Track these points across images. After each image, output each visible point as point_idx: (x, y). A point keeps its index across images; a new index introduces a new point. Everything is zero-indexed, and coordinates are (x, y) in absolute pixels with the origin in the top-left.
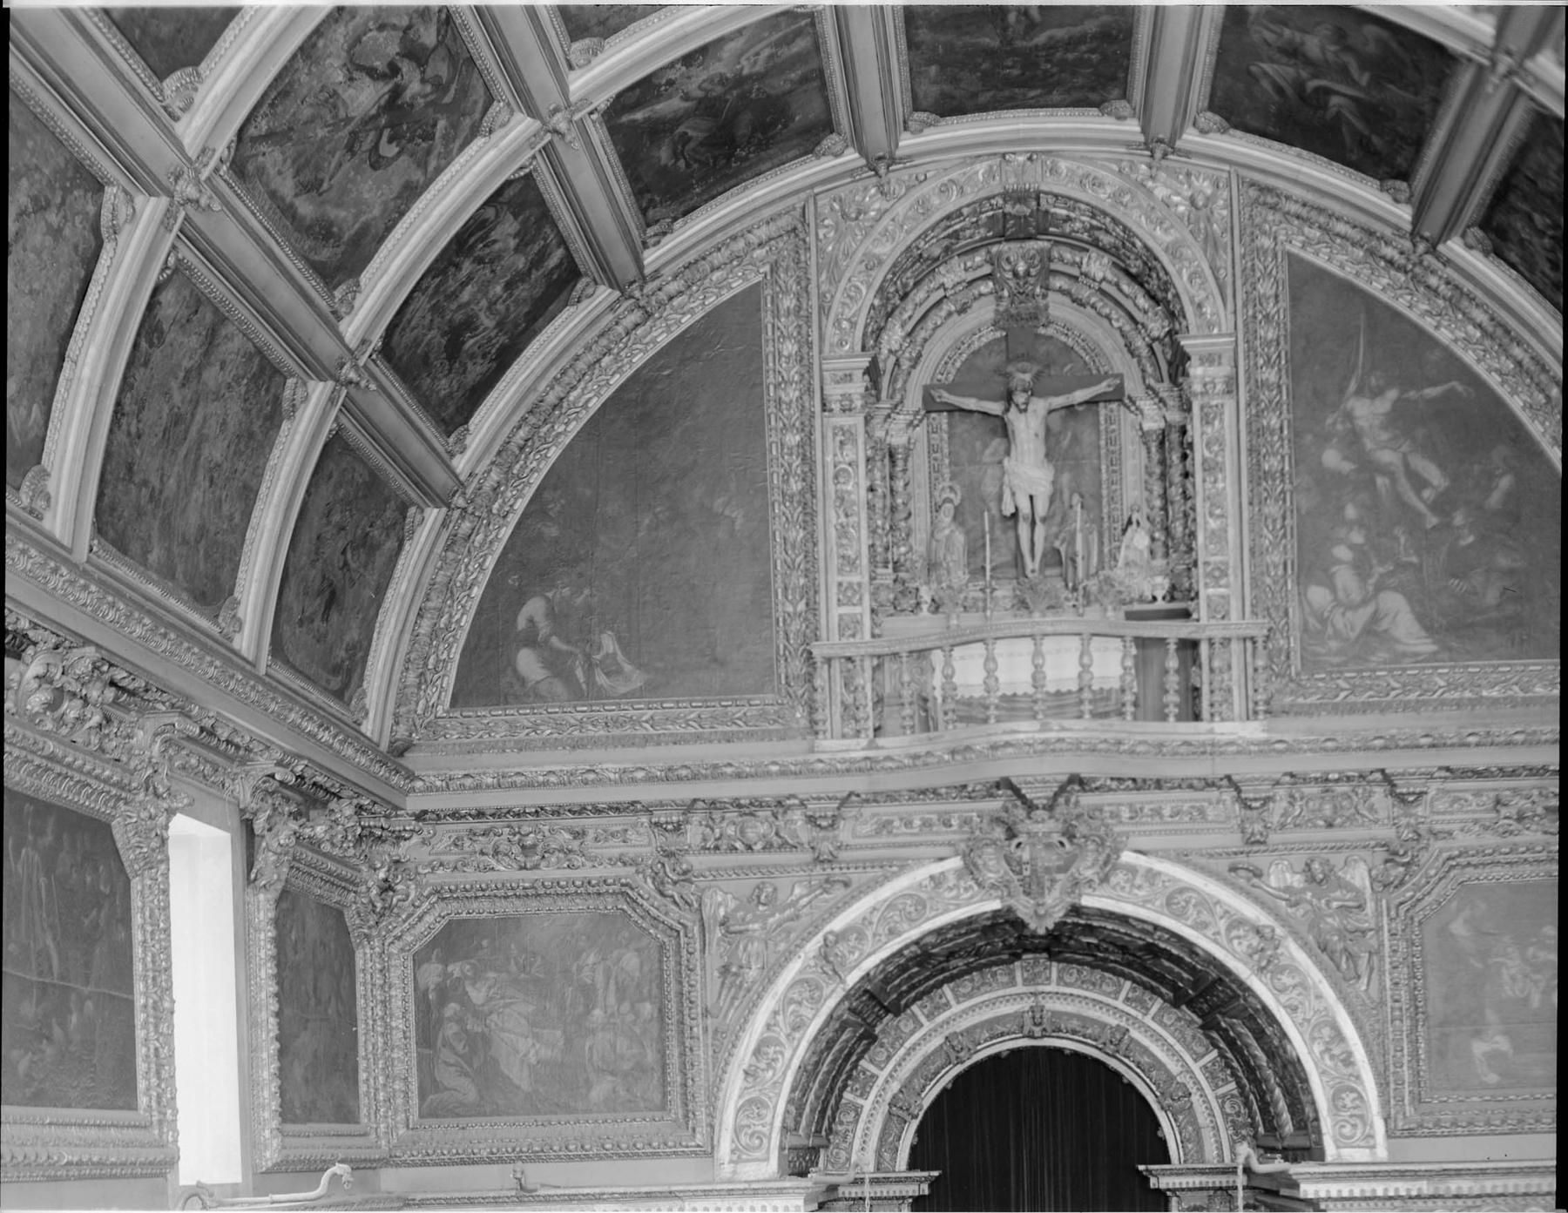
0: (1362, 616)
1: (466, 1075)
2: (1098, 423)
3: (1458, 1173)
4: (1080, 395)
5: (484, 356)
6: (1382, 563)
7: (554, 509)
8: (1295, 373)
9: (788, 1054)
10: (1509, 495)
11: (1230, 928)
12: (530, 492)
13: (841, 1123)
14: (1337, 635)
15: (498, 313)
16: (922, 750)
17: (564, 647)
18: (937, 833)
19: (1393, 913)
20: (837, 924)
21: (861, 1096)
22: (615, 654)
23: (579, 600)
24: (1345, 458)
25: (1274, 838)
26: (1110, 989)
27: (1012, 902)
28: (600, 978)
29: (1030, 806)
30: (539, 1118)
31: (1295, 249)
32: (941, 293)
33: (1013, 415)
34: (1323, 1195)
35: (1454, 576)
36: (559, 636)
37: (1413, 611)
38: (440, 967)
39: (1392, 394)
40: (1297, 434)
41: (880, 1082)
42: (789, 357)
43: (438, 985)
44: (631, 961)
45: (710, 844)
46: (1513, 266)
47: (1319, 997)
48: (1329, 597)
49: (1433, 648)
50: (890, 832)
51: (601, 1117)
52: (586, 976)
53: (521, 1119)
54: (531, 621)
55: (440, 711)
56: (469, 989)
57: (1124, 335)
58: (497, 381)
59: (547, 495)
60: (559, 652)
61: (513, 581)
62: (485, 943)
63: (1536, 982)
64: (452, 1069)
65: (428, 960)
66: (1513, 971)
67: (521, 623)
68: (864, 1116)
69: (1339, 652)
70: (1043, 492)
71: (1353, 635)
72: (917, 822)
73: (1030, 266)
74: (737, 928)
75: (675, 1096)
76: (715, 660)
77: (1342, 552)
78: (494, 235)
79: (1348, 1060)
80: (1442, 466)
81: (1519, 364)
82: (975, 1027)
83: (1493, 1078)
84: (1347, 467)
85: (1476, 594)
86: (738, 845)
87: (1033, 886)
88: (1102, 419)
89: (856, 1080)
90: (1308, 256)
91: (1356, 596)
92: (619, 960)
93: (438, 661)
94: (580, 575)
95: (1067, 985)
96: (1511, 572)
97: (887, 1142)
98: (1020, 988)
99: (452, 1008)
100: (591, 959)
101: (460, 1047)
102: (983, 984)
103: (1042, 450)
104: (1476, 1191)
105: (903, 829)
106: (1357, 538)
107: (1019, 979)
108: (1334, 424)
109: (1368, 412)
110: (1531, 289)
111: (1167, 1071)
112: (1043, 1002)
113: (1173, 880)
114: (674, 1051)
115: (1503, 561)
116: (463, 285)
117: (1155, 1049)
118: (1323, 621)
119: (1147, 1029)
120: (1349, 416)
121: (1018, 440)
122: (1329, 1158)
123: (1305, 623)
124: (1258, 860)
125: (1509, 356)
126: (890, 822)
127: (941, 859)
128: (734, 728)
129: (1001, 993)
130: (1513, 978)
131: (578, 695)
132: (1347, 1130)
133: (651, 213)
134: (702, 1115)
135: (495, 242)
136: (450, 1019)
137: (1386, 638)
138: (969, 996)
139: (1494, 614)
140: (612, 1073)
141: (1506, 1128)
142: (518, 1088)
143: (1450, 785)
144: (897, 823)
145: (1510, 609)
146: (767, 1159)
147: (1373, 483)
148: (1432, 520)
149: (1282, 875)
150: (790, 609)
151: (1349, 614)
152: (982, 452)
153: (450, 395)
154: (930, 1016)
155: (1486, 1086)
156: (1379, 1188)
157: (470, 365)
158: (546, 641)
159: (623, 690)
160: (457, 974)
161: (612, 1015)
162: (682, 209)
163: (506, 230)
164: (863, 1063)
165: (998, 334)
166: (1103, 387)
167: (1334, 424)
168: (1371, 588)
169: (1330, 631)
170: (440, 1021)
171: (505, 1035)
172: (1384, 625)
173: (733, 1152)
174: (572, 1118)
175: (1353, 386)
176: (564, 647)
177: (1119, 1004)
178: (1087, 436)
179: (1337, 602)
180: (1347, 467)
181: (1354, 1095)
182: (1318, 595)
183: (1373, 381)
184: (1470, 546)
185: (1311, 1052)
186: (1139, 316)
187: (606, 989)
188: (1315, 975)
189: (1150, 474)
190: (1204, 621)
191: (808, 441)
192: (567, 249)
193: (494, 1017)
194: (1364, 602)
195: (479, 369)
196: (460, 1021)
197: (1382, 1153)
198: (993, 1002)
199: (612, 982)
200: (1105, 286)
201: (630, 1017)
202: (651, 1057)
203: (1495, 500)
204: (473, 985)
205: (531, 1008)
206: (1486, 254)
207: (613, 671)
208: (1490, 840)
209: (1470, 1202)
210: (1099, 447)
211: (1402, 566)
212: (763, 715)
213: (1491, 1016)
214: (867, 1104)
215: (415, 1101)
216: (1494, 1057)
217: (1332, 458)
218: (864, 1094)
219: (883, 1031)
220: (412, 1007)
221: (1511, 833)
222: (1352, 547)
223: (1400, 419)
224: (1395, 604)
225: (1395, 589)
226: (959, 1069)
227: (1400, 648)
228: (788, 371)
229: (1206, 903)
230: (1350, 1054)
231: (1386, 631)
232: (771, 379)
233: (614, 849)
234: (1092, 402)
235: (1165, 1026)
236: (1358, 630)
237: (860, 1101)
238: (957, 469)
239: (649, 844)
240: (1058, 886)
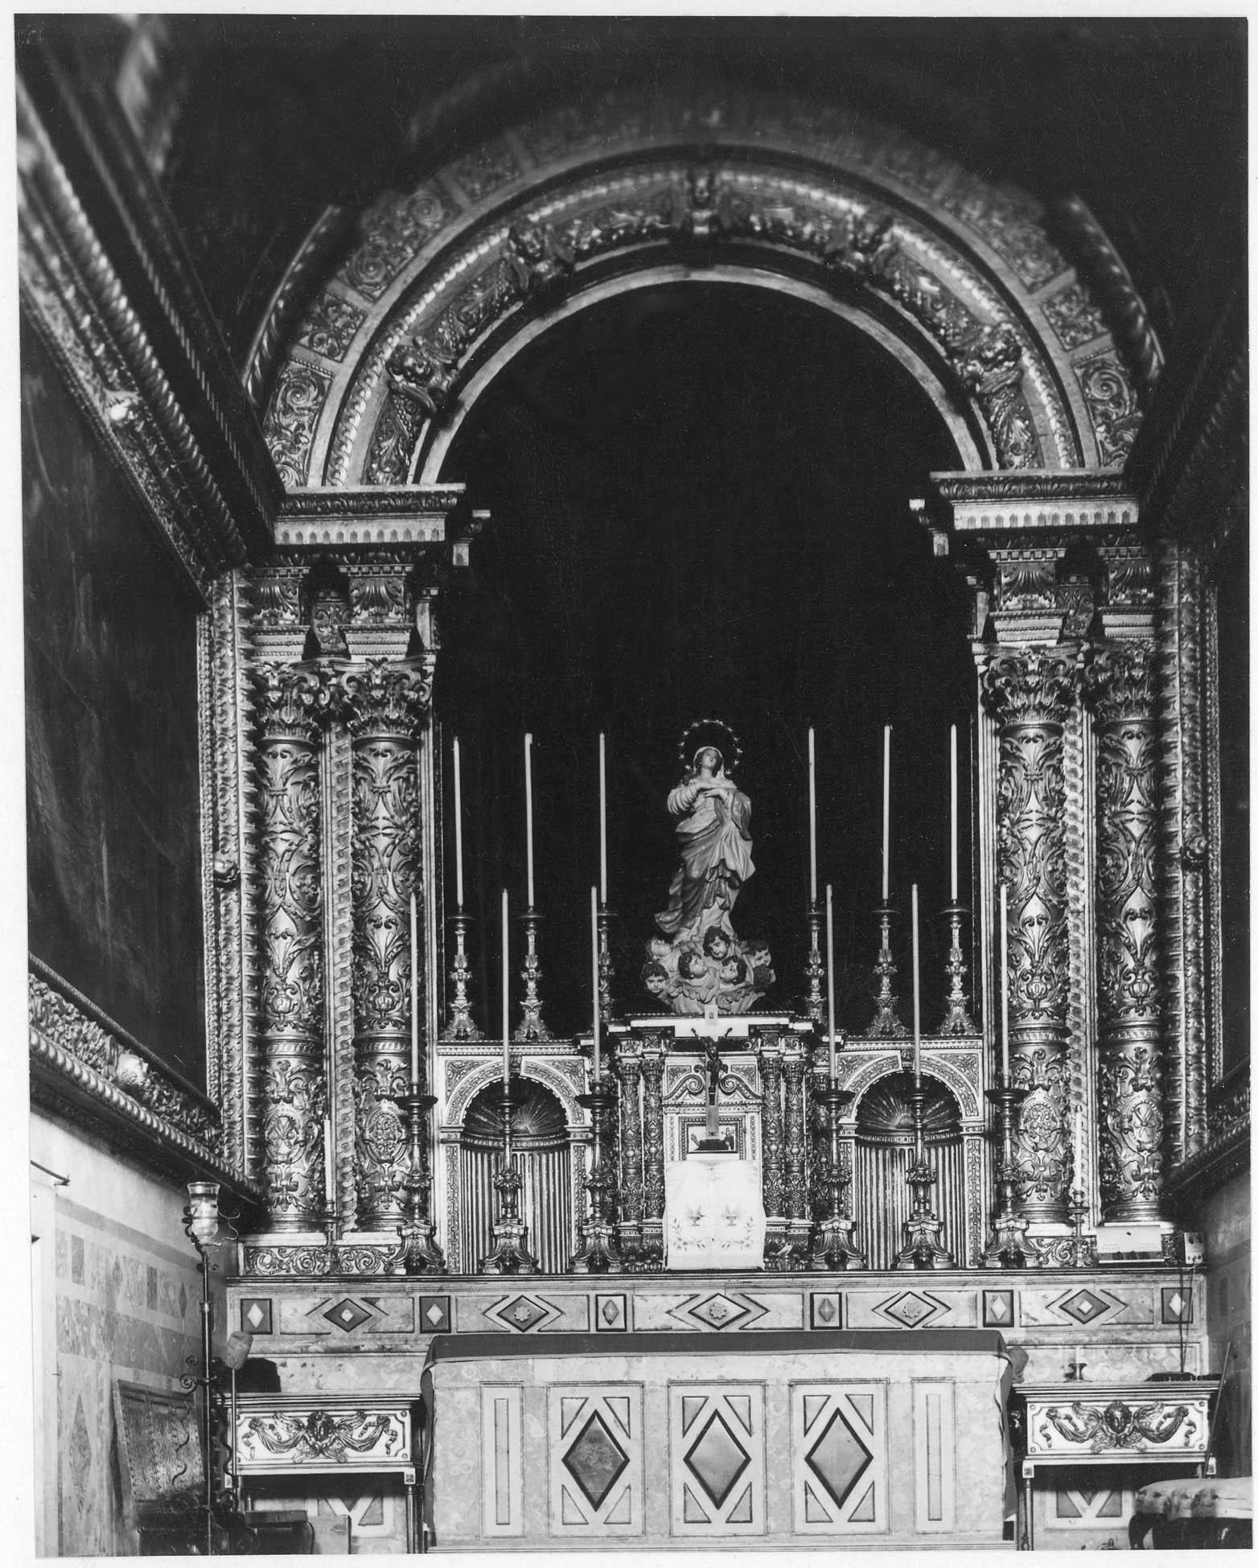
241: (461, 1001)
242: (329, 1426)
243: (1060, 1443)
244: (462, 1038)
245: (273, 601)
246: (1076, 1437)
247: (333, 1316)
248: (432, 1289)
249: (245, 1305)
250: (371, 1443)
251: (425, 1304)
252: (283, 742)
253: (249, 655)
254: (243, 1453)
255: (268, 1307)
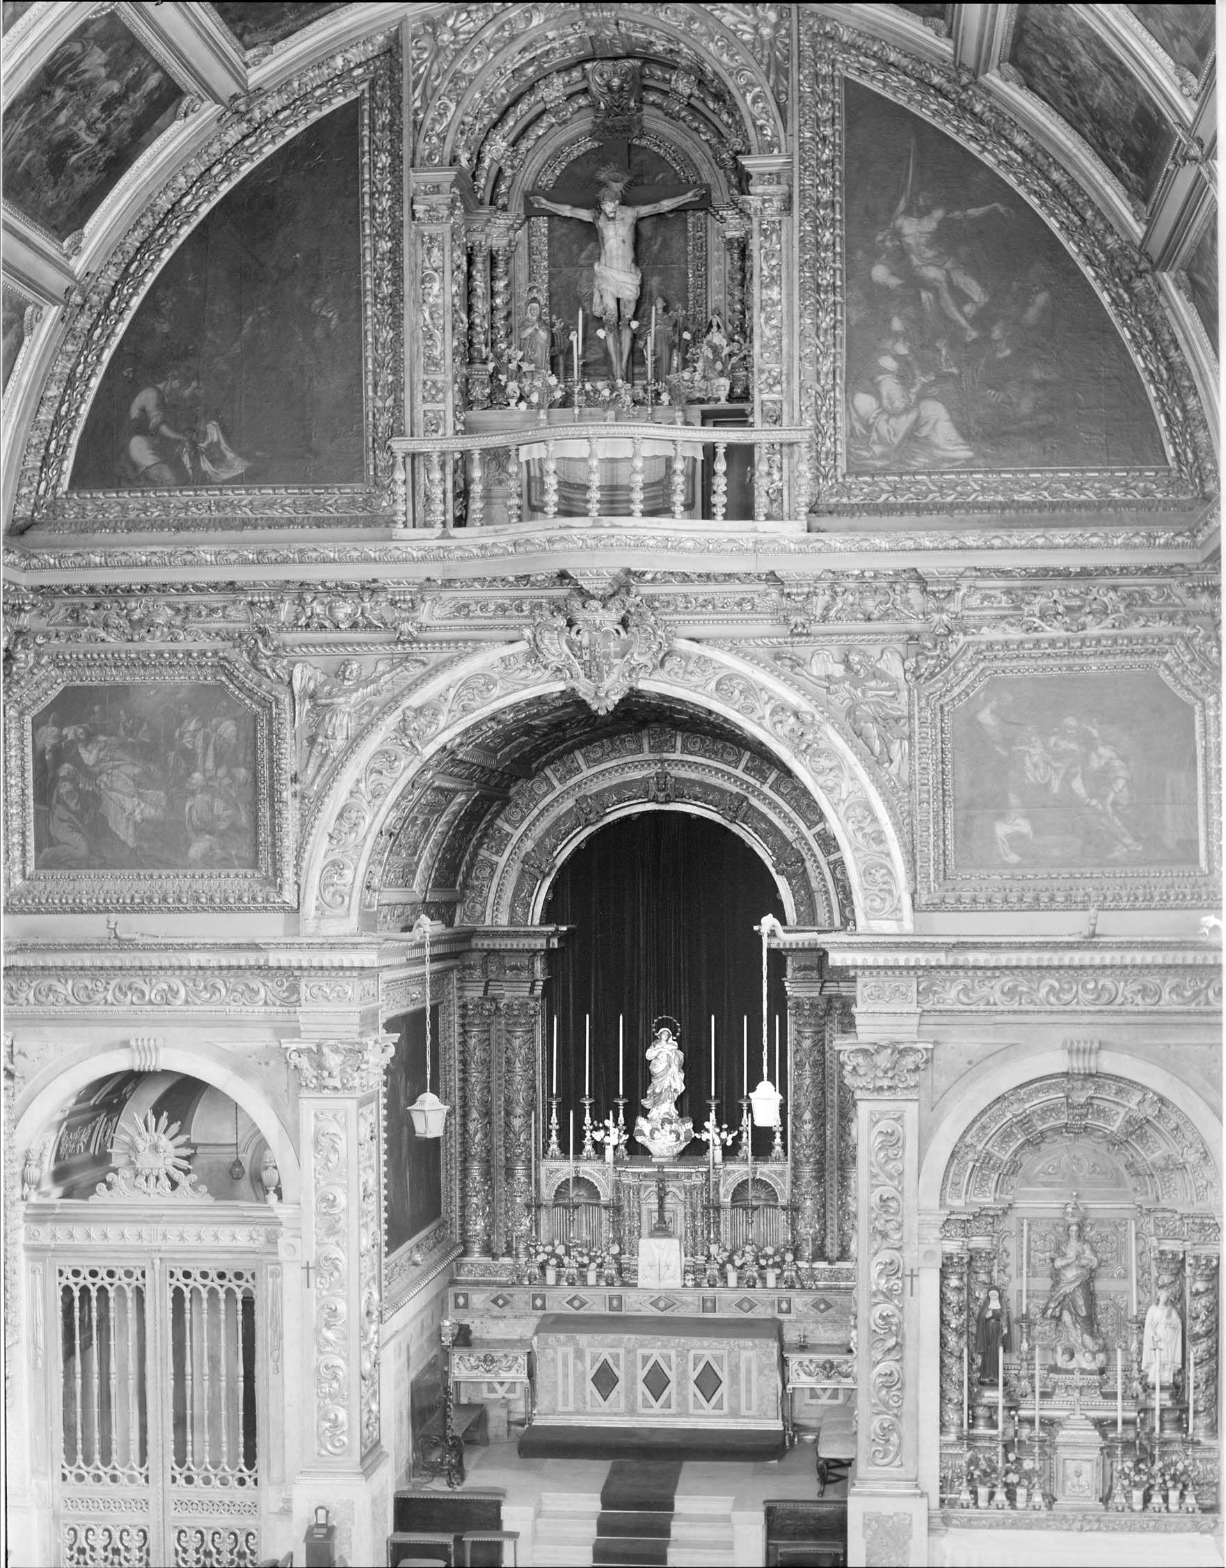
0: (904, 423)
1: (78, 831)
2: (687, 231)
3: (975, 946)
4: (667, 205)
5: (91, 168)
6: (924, 373)
7: (167, 306)
8: (849, 195)
9: (368, 820)
10: (1044, 310)
11: (773, 713)
12: (143, 291)
13: (477, 878)
14: (881, 440)
15: (98, 131)
16: (489, 541)
17: (173, 435)
18: (510, 617)
19: (923, 703)
20: (415, 700)
21: (497, 853)
22: (219, 442)
23: (187, 393)
24: (893, 274)
25: (815, 628)
26: (731, 759)
27: (575, 684)
28: (200, 743)
29: (585, 596)
30: (142, 872)
31: (853, 75)
32: (540, 107)
33: (601, 223)
34: (849, 963)
35: (991, 387)
36: (168, 425)
37: (953, 420)
38: (56, 730)
39: (938, 214)
40: (849, 250)
41: (514, 840)
42: (383, 168)
43: (54, 746)
44: (228, 728)
45: (303, 621)
46: (1043, 98)
47: (854, 779)
48: (875, 405)
49: (970, 454)
50: (467, 616)
51: (198, 872)
52: (187, 742)
53: (126, 872)
54: (143, 410)
55: (60, 490)
56: (82, 751)
57: (711, 146)
58: (104, 195)
59: (159, 294)
60: (168, 439)
61: (127, 372)
62: (97, 708)
63: (1056, 770)
64: (65, 825)
65: (45, 723)
66: (1035, 759)
67: (134, 412)
68: (498, 872)
69: (882, 456)
70: (630, 292)
71: (896, 441)
72: (492, 607)
73: (623, 81)
74: (323, 701)
75: (265, 856)
76: (310, 451)
77: (888, 362)
78: (82, 67)
79: (879, 838)
80: (984, 286)
81: (1056, 186)
82: (605, 790)
83: (1013, 858)
84: (894, 282)
85: (1011, 404)
86: (327, 623)
87: (593, 669)
88: (690, 228)
89: (492, 838)
90: (865, 82)
91: (899, 404)
92: (217, 727)
93: (58, 446)
94: (189, 368)
95: (691, 753)
96: (1043, 384)
97: (521, 900)
98: (646, 755)
99: (66, 769)
100: (192, 727)
101: (72, 805)
102: (613, 750)
103: (630, 255)
104: (992, 964)
105: (479, 613)
106: (902, 349)
107: (646, 747)
108: (883, 241)
109: (914, 230)
110: (1061, 120)
111: (783, 837)
112: (668, 769)
113: (723, 666)
114: (265, 812)
115: (1037, 374)
116: (59, 109)
117: (772, 816)
118: (868, 427)
119: (766, 797)
120: (898, 234)
121: (607, 247)
122: (859, 930)
123: (853, 429)
124: (803, 651)
125: (1048, 179)
126: (466, 606)
127: (512, 642)
128: (326, 514)
129: (629, 759)
130: (1036, 766)
131: (184, 481)
132: (877, 903)
133: (247, 38)
134: (289, 873)
135: (85, 71)
136: (64, 779)
137: (927, 443)
138: (598, 761)
139: (1027, 423)
140: (210, 833)
141: (1024, 906)
142: (124, 843)
143: (980, 583)
144: (472, 607)
145: (1043, 418)
146: (348, 915)
147: (919, 298)
148: (973, 334)
149: (825, 664)
150: (380, 404)
151: (892, 421)
152: (579, 255)
153: (59, 205)
154: (562, 780)
155: (1006, 865)
156: (902, 958)
157: (76, 177)
158: (157, 428)
159: (226, 476)
160: (70, 736)
161: (210, 779)
162: (279, 32)
163: (95, 61)
164: (499, 822)
165: (596, 144)
166: (689, 197)
167: (883, 241)
168: (913, 397)
169: (874, 436)
170: (56, 779)
171: (113, 794)
172: (925, 431)
173: (317, 908)
174: (172, 872)
175: (902, 205)
176: (173, 435)
177: (738, 772)
178: (677, 244)
179: (882, 409)
180: (894, 282)
181: (884, 871)
182: (864, 402)
183: (921, 202)
184: (1006, 359)
185: (845, 831)
186: (724, 130)
187: (205, 754)
188: (851, 758)
189: (732, 279)
190: (758, 425)
191: (396, 251)
192: (164, 72)
193: (104, 777)
194: (907, 410)
195: (87, 180)
196: (73, 780)
197: (908, 926)
198: (622, 767)
199: (211, 747)
200: (693, 101)
201: (227, 781)
202: (244, 820)
203: (1032, 314)
204: (86, 747)
205: (137, 770)
206: (1021, 86)
207: (217, 459)
208: (1015, 634)
209: (989, 973)
210: (687, 253)
211: (943, 377)
212: (352, 503)
213: (1014, 800)
214: (502, 861)
215: (31, 853)
216: (1016, 839)
217: (880, 273)
218: (499, 852)
219: (517, 793)
220: (30, 766)
221: (1036, 629)
222: (897, 358)
223: (945, 238)
224: (936, 413)
225: (936, 398)
226: (589, 830)
227: (939, 453)
228: (382, 181)
229: (751, 690)
230: (881, 832)
231: (926, 437)
232: (366, 189)
233: (217, 623)
234: (681, 210)
235: (781, 795)
236: (901, 435)
237: (495, 858)
238: (554, 270)
239: (248, 621)
240: (615, 670)
241: (554, 1138)
242: (492, 1361)
243: (804, 1377)
244: (554, 1158)
245: (470, 967)
246: (810, 1375)
247: (495, 1301)
248: (538, 1291)
249: (456, 1296)
250: (510, 1368)
251: (534, 1297)
252: (475, 1031)
253: (461, 989)
254: (456, 1371)
255: (466, 1296)
